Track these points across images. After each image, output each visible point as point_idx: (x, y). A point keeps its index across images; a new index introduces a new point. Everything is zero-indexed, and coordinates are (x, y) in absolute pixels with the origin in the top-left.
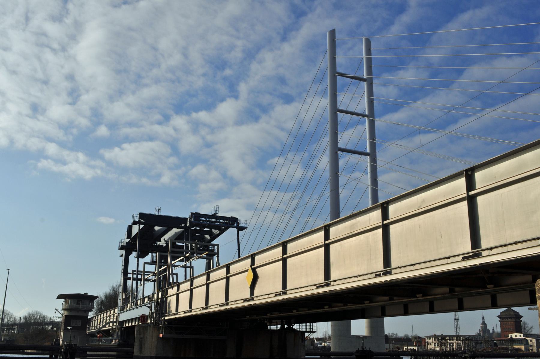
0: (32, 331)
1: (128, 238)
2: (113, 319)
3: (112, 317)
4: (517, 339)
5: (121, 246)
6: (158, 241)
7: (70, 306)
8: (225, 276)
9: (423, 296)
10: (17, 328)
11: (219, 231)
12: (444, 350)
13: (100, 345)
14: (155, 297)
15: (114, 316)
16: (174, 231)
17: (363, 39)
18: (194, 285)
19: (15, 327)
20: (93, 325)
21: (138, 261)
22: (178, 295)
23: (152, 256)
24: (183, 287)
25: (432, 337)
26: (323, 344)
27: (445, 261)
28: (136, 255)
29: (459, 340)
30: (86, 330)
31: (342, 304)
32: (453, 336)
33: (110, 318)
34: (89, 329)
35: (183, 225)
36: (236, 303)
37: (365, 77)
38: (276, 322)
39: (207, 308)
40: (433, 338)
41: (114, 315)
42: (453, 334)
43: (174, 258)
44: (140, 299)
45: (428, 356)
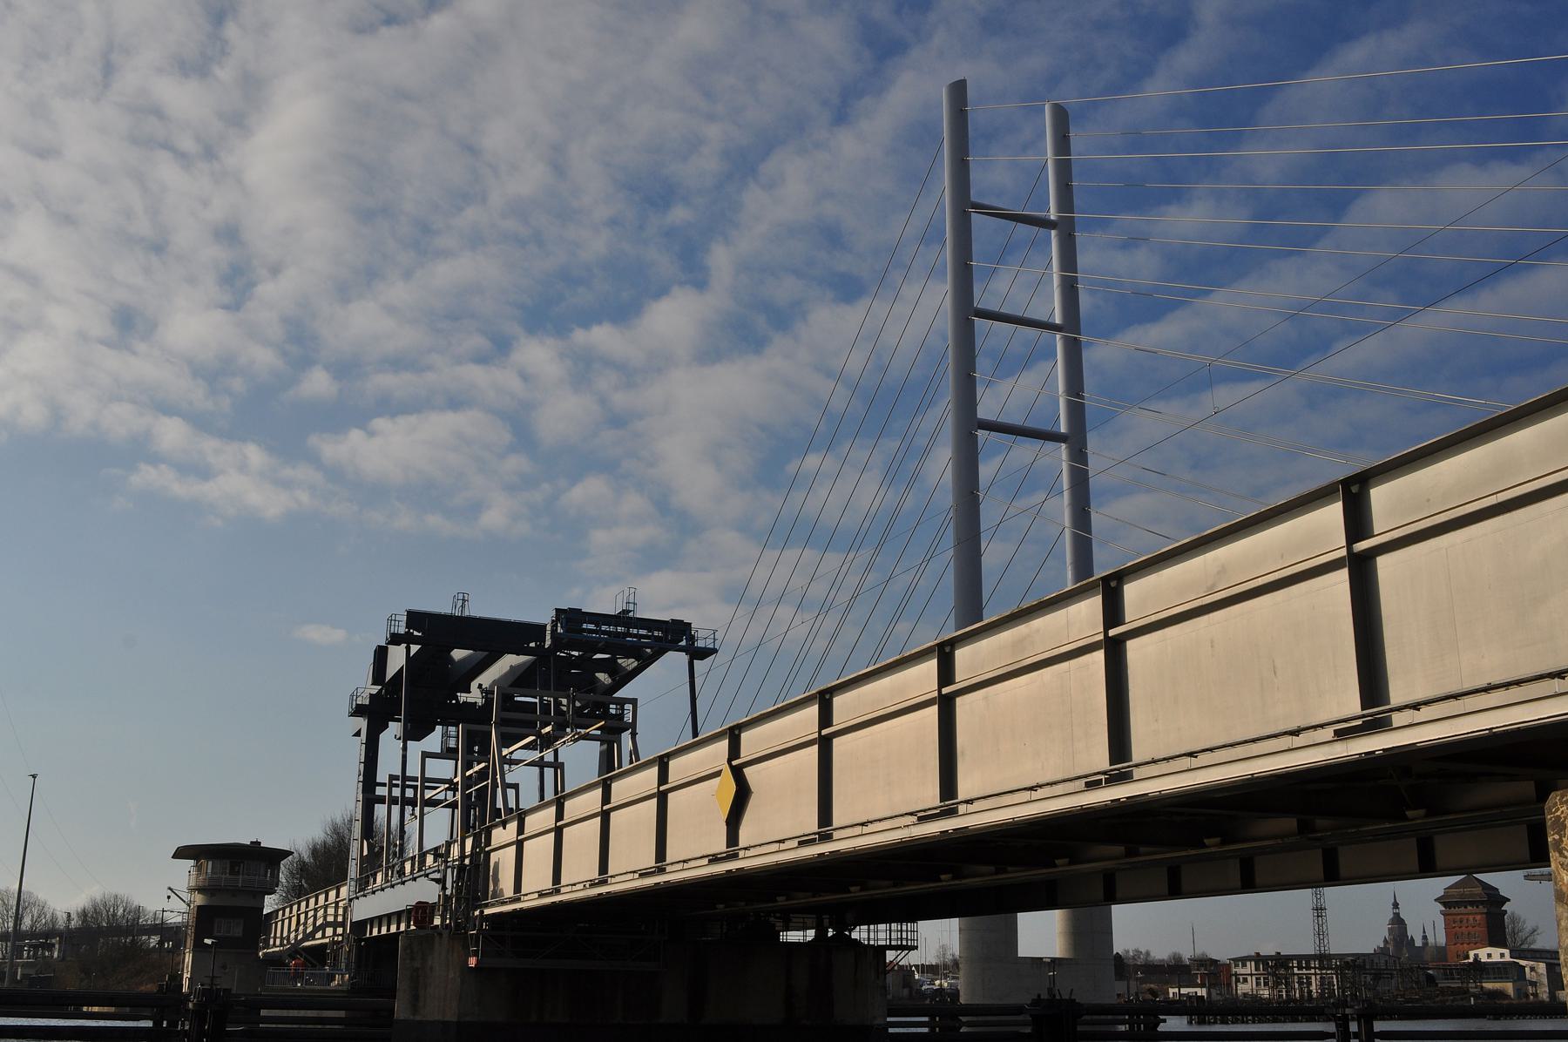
2: (336, 916)
3: (331, 911)
10: (60, 943)
13: (299, 990)
14: (455, 851)
15: (337, 908)
17: (1047, 108)
18: (565, 818)
19: (53, 941)
20: (278, 935)
21: (405, 749)
22: (519, 845)
23: (445, 735)
24: (534, 822)
25: (1250, 961)
26: (937, 982)
29: (1328, 969)
30: (258, 949)
32: (1308, 958)
33: (326, 911)
35: (532, 645)
39: (604, 882)
40: (1253, 963)
41: (337, 903)
42: (1310, 950)
43: (507, 740)
44: (413, 858)
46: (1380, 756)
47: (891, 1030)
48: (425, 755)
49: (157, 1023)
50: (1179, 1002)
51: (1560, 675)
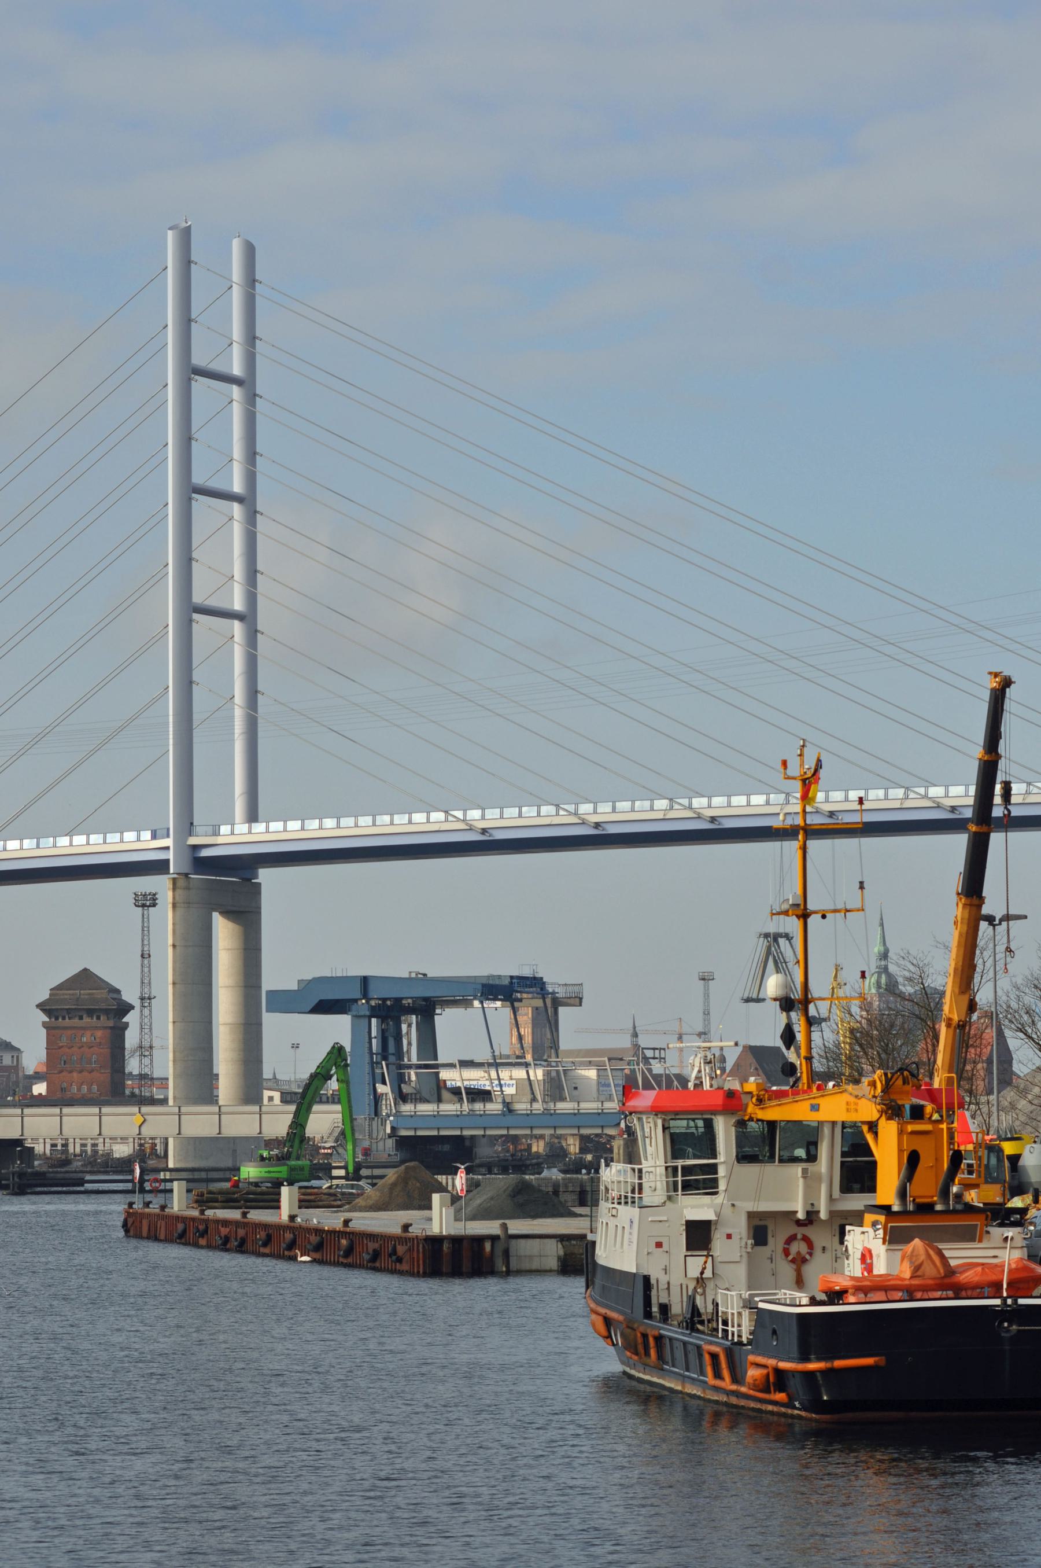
4: (149, 1215)
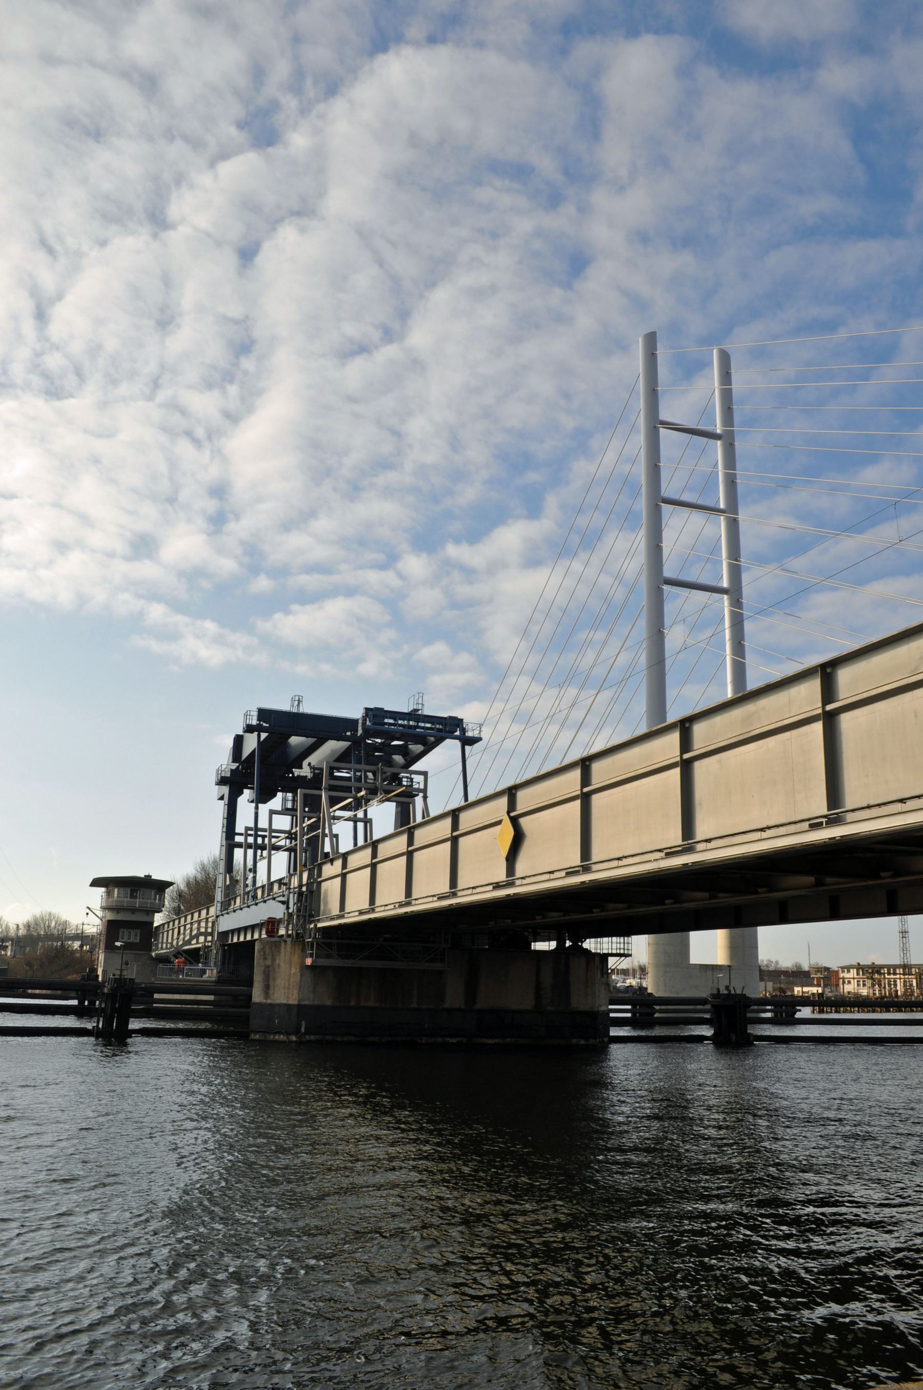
0: (42, 951)
1: (234, 761)
2: (206, 928)
3: (203, 924)
5: (222, 777)
6: (296, 768)
7: (116, 901)
8: (450, 836)
9: (894, 876)
10: (12, 945)
11: (424, 746)
12: (877, 994)
13: (181, 980)
14: (295, 882)
15: (207, 922)
16: (332, 747)
17: (715, 352)
18: (378, 856)
19: (7, 944)
20: (165, 940)
21: (257, 808)
22: (344, 876)
23: (285, 800)
24: (355, 861)
25: (853, 968)
26: (628, 981)
27: (615, 863)
28: (253, 796)
29: (909, 975)
30: (150, 950)
31: (706, 895)
32: (895, 967)
33: (199, 924)
34: (157, 949)
35: (349, 733)
36: (475, 891)
37: (719, 431)
38: (547, 934)
39: (408, 904)
40: (855, 970)
41: (207, 919)
42: (897, 961)
43: (333, 801)
44: (263, 887)
45: (847, 1006)
46: (838, 840)
47: (612, 1015)
48: (272, 812)
49: (81, 1002)
50: (802, 997)
51: (919, 797)
